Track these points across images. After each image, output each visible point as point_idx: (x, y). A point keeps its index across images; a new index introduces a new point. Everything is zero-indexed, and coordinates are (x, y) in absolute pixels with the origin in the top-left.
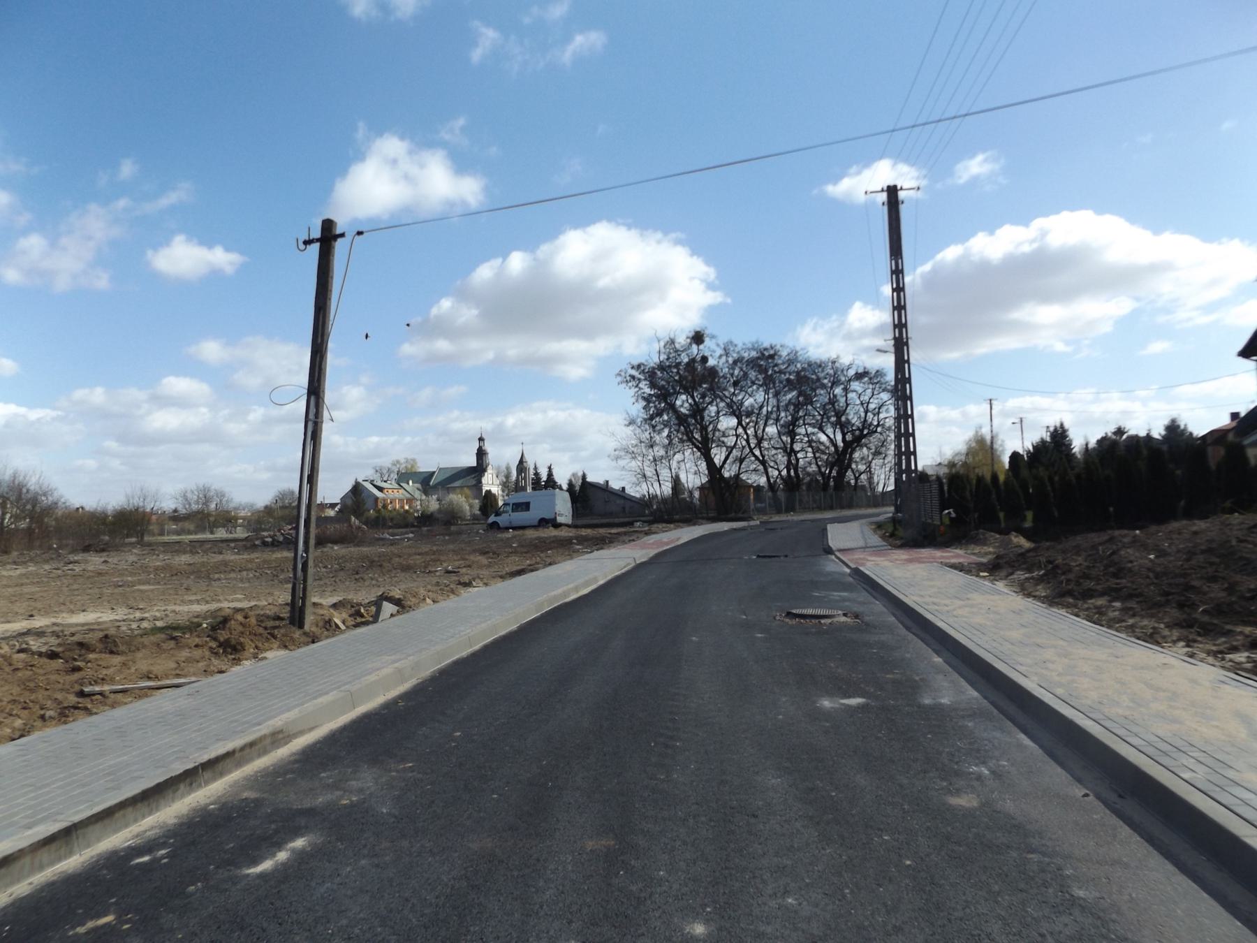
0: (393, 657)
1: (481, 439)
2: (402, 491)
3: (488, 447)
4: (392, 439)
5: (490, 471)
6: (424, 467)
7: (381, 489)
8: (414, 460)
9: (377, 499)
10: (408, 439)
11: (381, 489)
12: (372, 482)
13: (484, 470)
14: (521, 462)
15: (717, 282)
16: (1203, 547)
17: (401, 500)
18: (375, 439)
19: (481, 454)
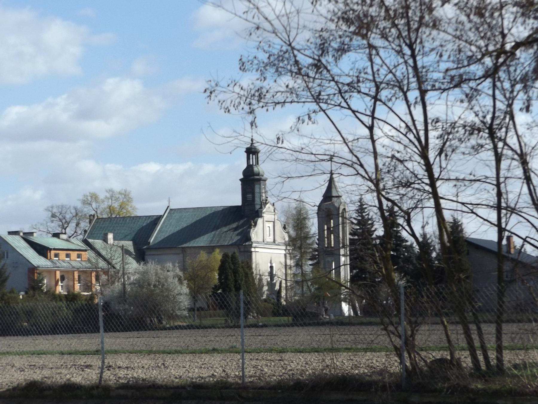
0: (358, 309)
1: (251, 151)
2: (89, 254)
3: (264, 168)
4: (181, 168)
5: (268, 214)
6: (145, 208)
7: (42, 250)
8: (125, 194)
9: (33, 269)
10: (208, 168)
11: (42, 250)
12: (27, 237)
13: (258, 214)
14: (328, 196)
15: (450, 232)
16: (526, 168)
17: (84, 274)
18: (153, 168)
19: (251, 180)
